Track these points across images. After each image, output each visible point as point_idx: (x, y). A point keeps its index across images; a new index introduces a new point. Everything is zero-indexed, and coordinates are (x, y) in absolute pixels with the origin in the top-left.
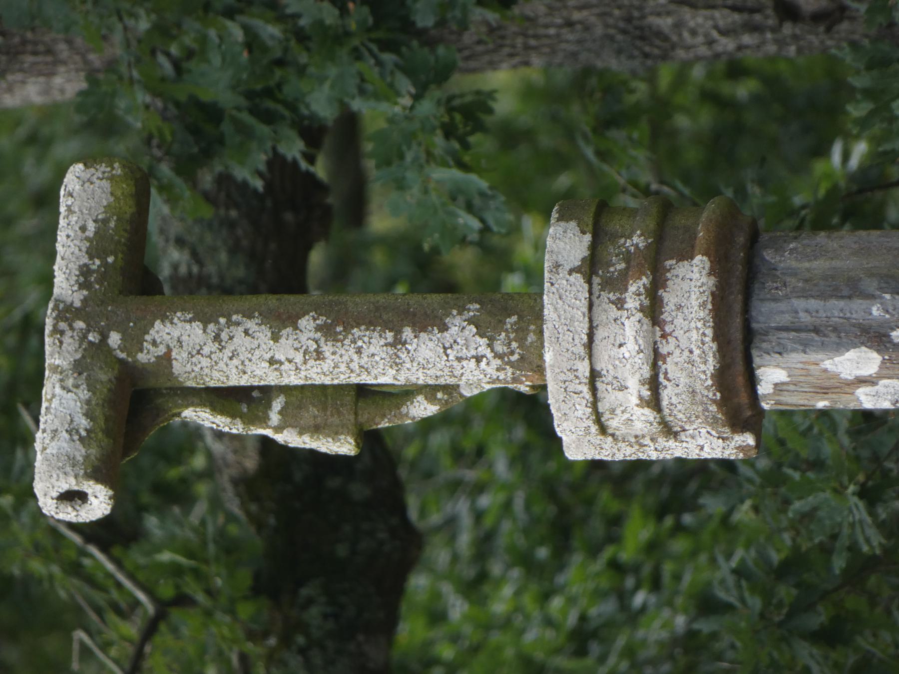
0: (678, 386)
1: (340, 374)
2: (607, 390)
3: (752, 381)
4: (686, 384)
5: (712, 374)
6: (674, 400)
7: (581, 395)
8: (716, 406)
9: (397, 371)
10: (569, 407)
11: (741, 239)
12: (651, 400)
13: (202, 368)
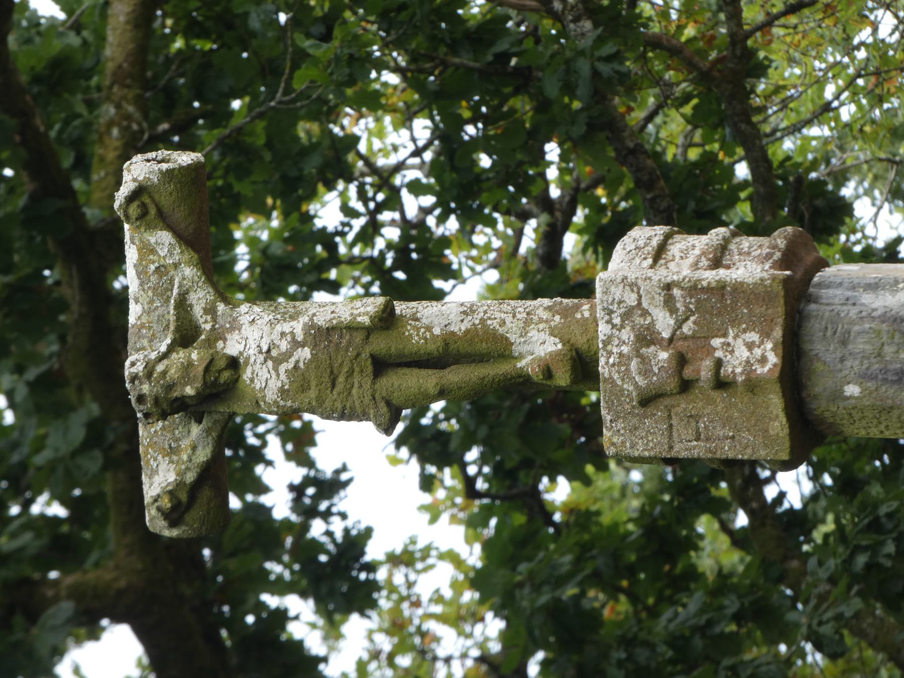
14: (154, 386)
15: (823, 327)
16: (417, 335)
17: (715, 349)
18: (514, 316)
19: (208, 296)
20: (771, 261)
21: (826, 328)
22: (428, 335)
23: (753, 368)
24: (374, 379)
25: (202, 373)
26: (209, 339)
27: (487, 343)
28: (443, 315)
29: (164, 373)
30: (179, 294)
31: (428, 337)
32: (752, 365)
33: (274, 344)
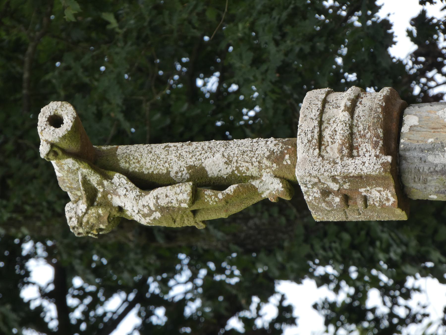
0: (365, 107)
1: (197, 152)
2: (329, 108)
3: (400, 123)
4: (369, 105)
5: (384, 95)
6: (361, 114)
7: (317, 105)
8: (381, 109)
9: (226, 149)
10: (309, 112)
11: (400, 182)
12: (350, 108)
13: (131, 151)
14: (85, 228)
15: (413, 177)
16: (212, 200)
17: (362, 193)
18: (252, 165)
19: (97, 178)
20: (379, 148)
21: (415, 178)
22: (216, 199)
23: (384, 203)
24: (194, 216)
25: (107, 220)
26: (103, 196)
27: (246, 194)
28: (216, 165)
29: (88, 222)
30: (83, 178)
31: (217, 200)
32: (383, 202)
33: (140, 210)
